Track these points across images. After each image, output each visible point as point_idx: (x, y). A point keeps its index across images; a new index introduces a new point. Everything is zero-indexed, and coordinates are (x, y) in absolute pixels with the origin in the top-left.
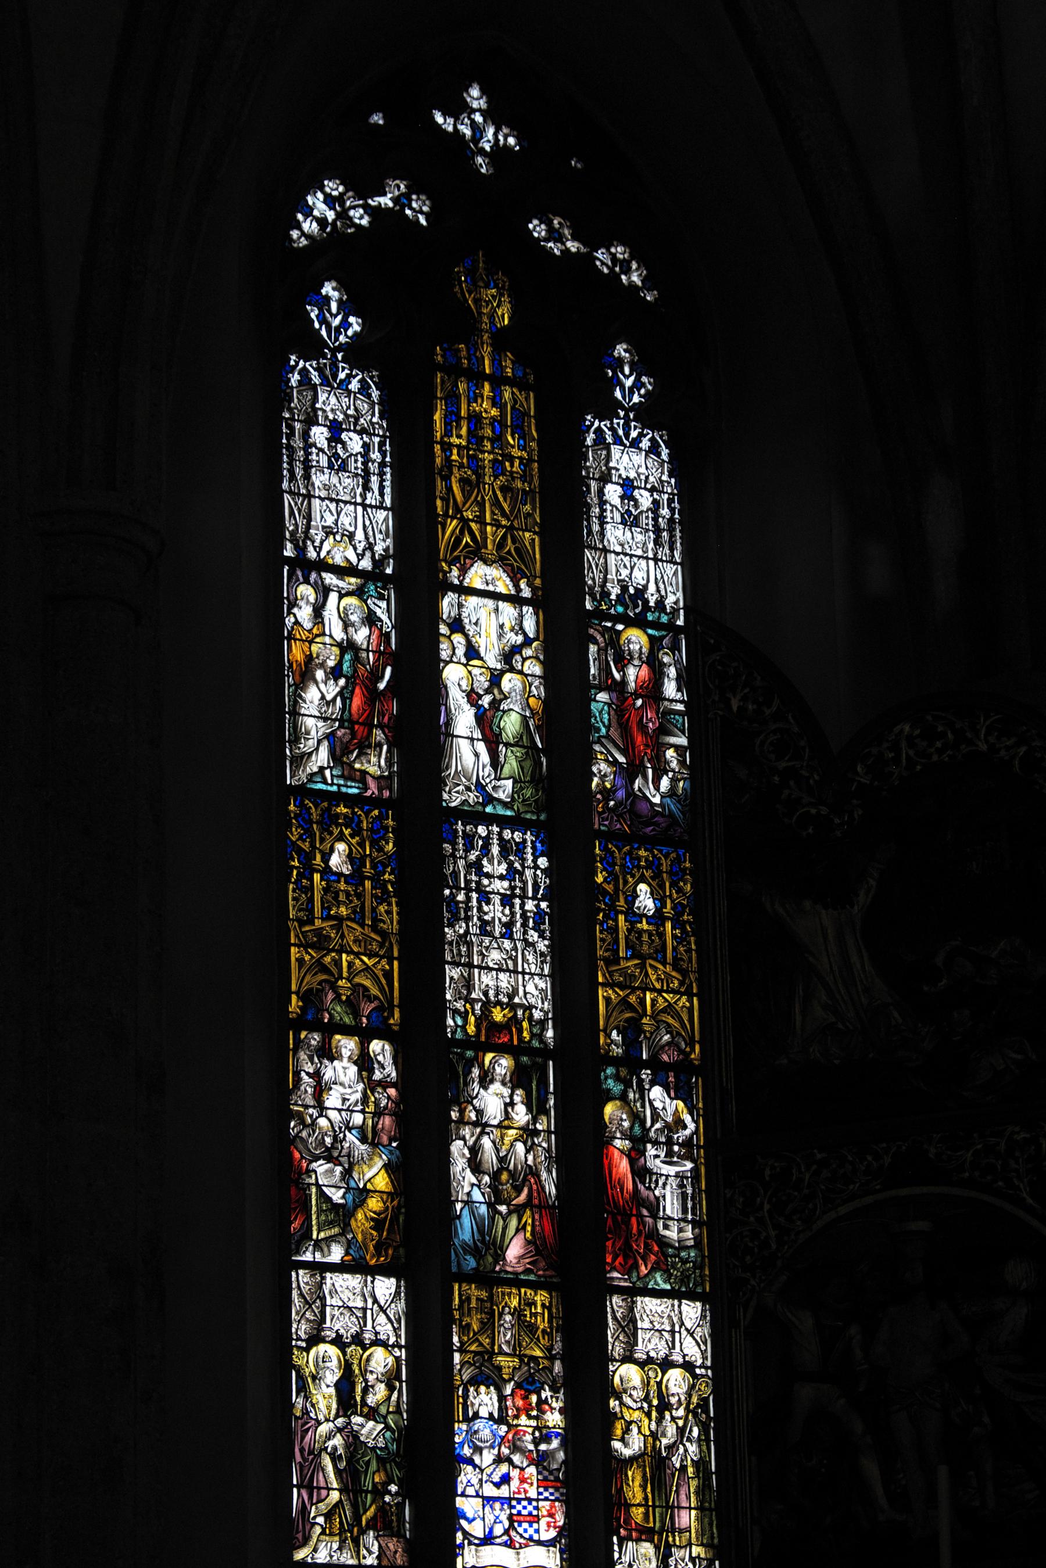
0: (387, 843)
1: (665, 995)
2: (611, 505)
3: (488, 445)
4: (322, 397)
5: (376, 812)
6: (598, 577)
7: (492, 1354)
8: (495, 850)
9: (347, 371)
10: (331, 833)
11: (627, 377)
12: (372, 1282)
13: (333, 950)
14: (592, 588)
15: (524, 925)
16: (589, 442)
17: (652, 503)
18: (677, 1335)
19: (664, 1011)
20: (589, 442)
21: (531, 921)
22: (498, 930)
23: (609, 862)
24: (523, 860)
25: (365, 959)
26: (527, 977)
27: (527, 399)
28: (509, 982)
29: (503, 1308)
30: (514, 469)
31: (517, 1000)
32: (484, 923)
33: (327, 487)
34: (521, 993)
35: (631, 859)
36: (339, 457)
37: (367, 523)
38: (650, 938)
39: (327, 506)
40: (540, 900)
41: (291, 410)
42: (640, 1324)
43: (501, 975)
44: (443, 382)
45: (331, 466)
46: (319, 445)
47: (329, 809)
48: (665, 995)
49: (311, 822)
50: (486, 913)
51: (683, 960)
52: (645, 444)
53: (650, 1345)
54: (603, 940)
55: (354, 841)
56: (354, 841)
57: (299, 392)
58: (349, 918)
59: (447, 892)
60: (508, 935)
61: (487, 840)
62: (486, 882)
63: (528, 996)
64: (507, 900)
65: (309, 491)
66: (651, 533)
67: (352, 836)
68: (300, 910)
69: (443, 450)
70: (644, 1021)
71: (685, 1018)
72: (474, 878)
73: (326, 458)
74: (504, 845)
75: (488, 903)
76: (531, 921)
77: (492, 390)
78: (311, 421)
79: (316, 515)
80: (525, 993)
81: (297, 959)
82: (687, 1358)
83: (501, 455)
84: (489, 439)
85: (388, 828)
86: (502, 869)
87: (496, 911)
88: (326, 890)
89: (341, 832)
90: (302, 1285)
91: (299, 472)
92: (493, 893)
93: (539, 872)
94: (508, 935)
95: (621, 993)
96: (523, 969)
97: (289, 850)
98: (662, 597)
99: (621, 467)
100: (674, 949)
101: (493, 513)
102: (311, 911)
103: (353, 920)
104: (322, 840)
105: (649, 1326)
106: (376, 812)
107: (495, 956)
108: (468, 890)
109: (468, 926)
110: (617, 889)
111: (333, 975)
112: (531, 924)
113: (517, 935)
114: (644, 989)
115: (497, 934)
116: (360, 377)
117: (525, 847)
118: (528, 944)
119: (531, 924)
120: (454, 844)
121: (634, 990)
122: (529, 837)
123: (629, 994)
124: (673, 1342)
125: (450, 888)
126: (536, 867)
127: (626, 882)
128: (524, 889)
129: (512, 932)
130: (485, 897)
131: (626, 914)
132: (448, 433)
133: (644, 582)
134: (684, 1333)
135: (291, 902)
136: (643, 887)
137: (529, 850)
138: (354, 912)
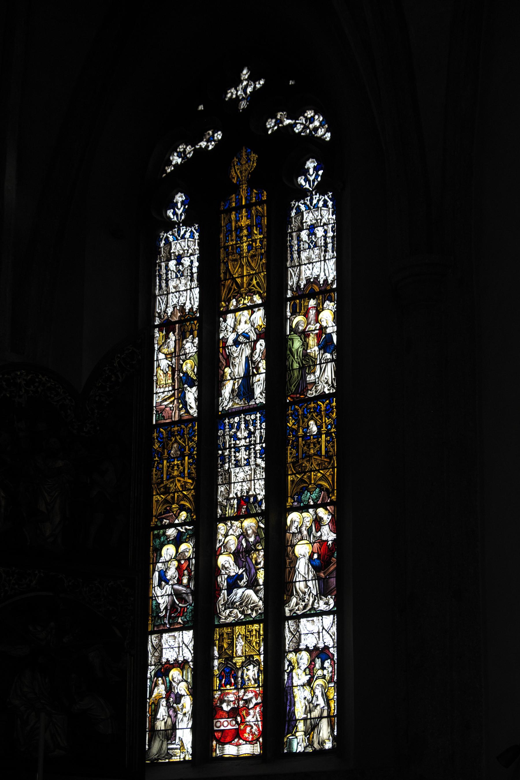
0: (333, 414)
1: (321, 471)
2: (171, 271)
3: (245, 239)
4: (305, 215)
5: (328, 401)
6: (295, 279)
7: (233, 658)
8: (243, 426)
9: (185, 230)
10: (171, 440)
11: (311, 176)
12: (322, 620)
13: (172, 493)
14: (159, 314)
15: (255, 457)
16: (293, 214)
17: (324, 232)
18: (321, 634)
19: (320, 479)
20: (293, 214)
21: (258, 454)
22: (244, 462)
23: (295, 415)
24: (255, 427)
25: (162, 496)
26: (256, 481)
27: (263, 209)
28: (247, 486)
29: (238, 636)
30: (257, 245)
31: (251, 493)
32: (237, 461)
33: (175, 287)
34: (253, 489)
35: (307, 409)
36: (313, 241)
37: (191, 295)
38: (178, 467)
39: (308, 267)
40: (263, 443)
41: (291, 228)
42: (164, 646)
43: (244, 484)
44: (224, 218)
45: (177, 277)
46: (172, 269)
47: (171, 430)
48: (321, 471)
49: (299, 415)
50: (237, 457)
51: (331, 451)
52: (188, 235)
53: (309, 641)
54: (156, 475)
55: (318, 418)
56: (318, 418)
57: (295, 218)
58: (178, 476)
59: (220, 452)
60: (248, 464)
61: (239, 424)
62: (238, 442)
63: (256, 490)
64: (247, 448)
65: (299, 263)
66: (323, 247)
67: (317, 416)
68: (292, 458)
69: (225, 250)
70: (310, 486)
71: (330, 479)
72: (233, 442)
73: (175, 274)
74: (247, 422)
75: (239, 452)
76: (258, 454)
77: (247, 212)
78: (301, 229)
79: (170, 301)
80: (255, 489)
81: (291, 481)
82: (326, 644)
83: (251, 241)
84: (245, 236)
85: (333, 407)
86: (246, 434)
87: (243, 455)
88: (168, 467)
89: (176, 439)
90: (153, 641)
91: (164, 285)
92: (242, 446)
93: (262, 431)
94: (248, 464)
95: (163, 497)
96: (254, 478)
97: (154, 453)
98: (327, 277)
99: (308, 220)
100: (326, 447)
101: (247, 270)
102: (162, 478)
103: (180, 476)
104: (303, 422)
105: (169, 647)
106: (328, 401)
107: (241, 475)
108: (230, 448)
109: (229, 465)
110: (299, 427)
111: (307, 483)
112: (258, 456)
113: (252, 463)
114: (311, 471)
115: (243, 465)
116: (190, 230)
117: (256, 420)
118: (257, 465)
119: (258, 456)
120: (224, 429)
121: (305, 473)
122: (258, 415)
123: (304, 475)
124: (319, 638)
125: (221, 450)
126: (261, 428)
127: (303, 422)
128: (255, 441)
129: (249, 462)
130: (238, 449)
131: (167, 459)
132: (226, 241)
133: (318, 274)
134: (184, 646)
135: (289, 455)
136: (312, 422)
137: (258, 421)
138: (180, 473)
